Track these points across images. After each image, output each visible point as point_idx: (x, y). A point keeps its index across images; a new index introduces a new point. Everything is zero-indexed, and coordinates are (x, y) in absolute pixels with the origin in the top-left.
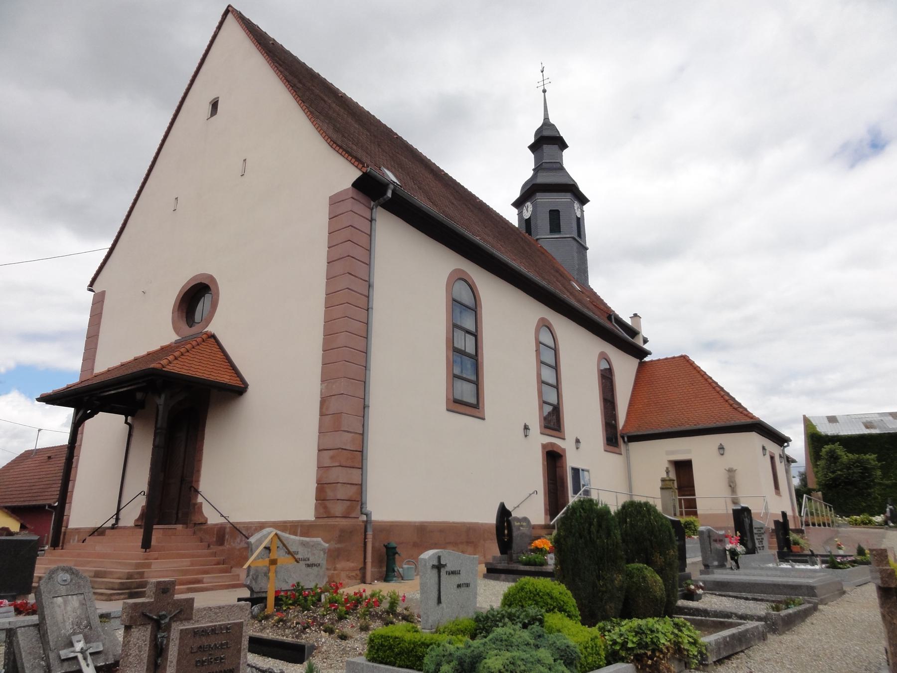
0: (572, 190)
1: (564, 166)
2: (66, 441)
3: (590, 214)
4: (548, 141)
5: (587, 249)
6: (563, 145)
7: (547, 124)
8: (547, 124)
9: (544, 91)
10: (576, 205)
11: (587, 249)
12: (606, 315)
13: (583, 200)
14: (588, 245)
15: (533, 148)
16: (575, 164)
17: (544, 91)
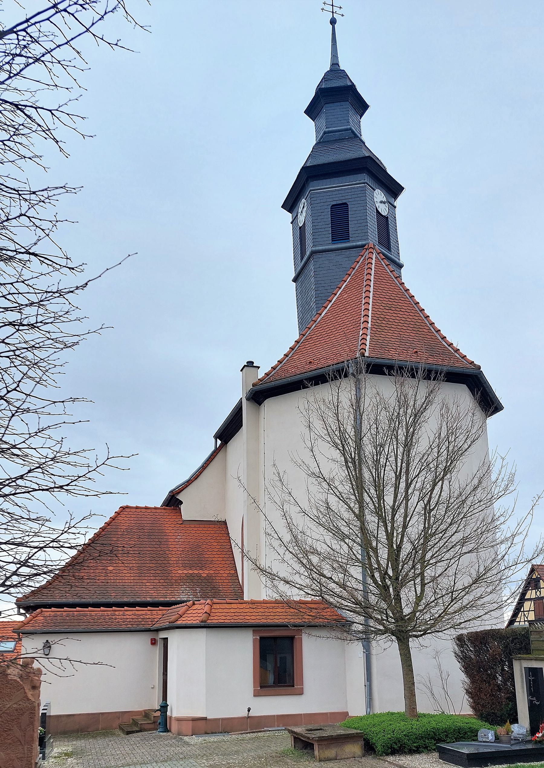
0: (372, 170)
1: (363, 138)
2: (413, 643)
3: (407, 214)
4: (336, 97)
5: (401, 266)
6: (362, 107)
7: (335, 71)
8: (335, 71)
9: (333, 22)
10: (379, 195)
11: (401, 266)
12: (356, 749)
13: (393, 189)
14: (403, 259)
15: (312, 111)
16: (377, 134)
17: (333, 22)
